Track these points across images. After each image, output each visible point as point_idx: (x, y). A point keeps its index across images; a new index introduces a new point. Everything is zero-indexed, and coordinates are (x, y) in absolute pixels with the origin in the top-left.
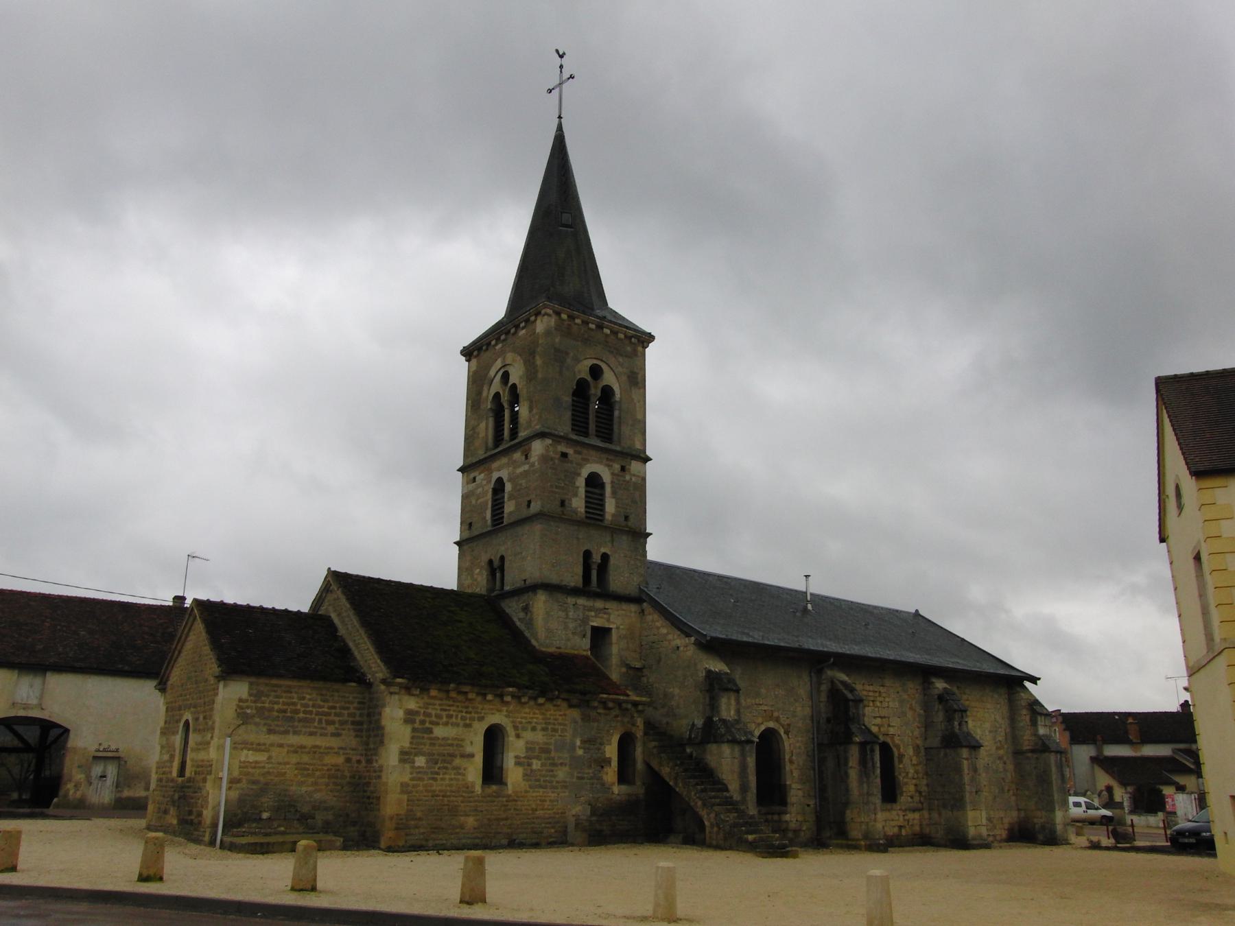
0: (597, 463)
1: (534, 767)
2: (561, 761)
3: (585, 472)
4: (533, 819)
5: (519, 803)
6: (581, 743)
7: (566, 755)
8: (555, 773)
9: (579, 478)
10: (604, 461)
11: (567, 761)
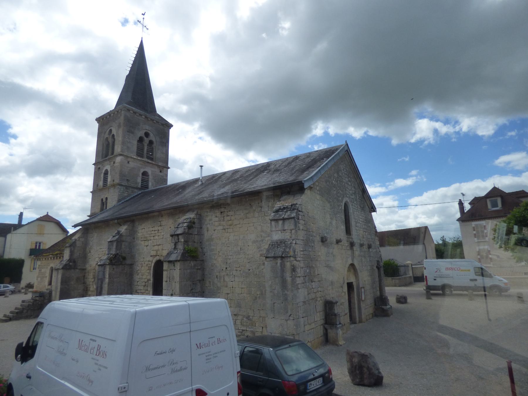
3: (142, 171)
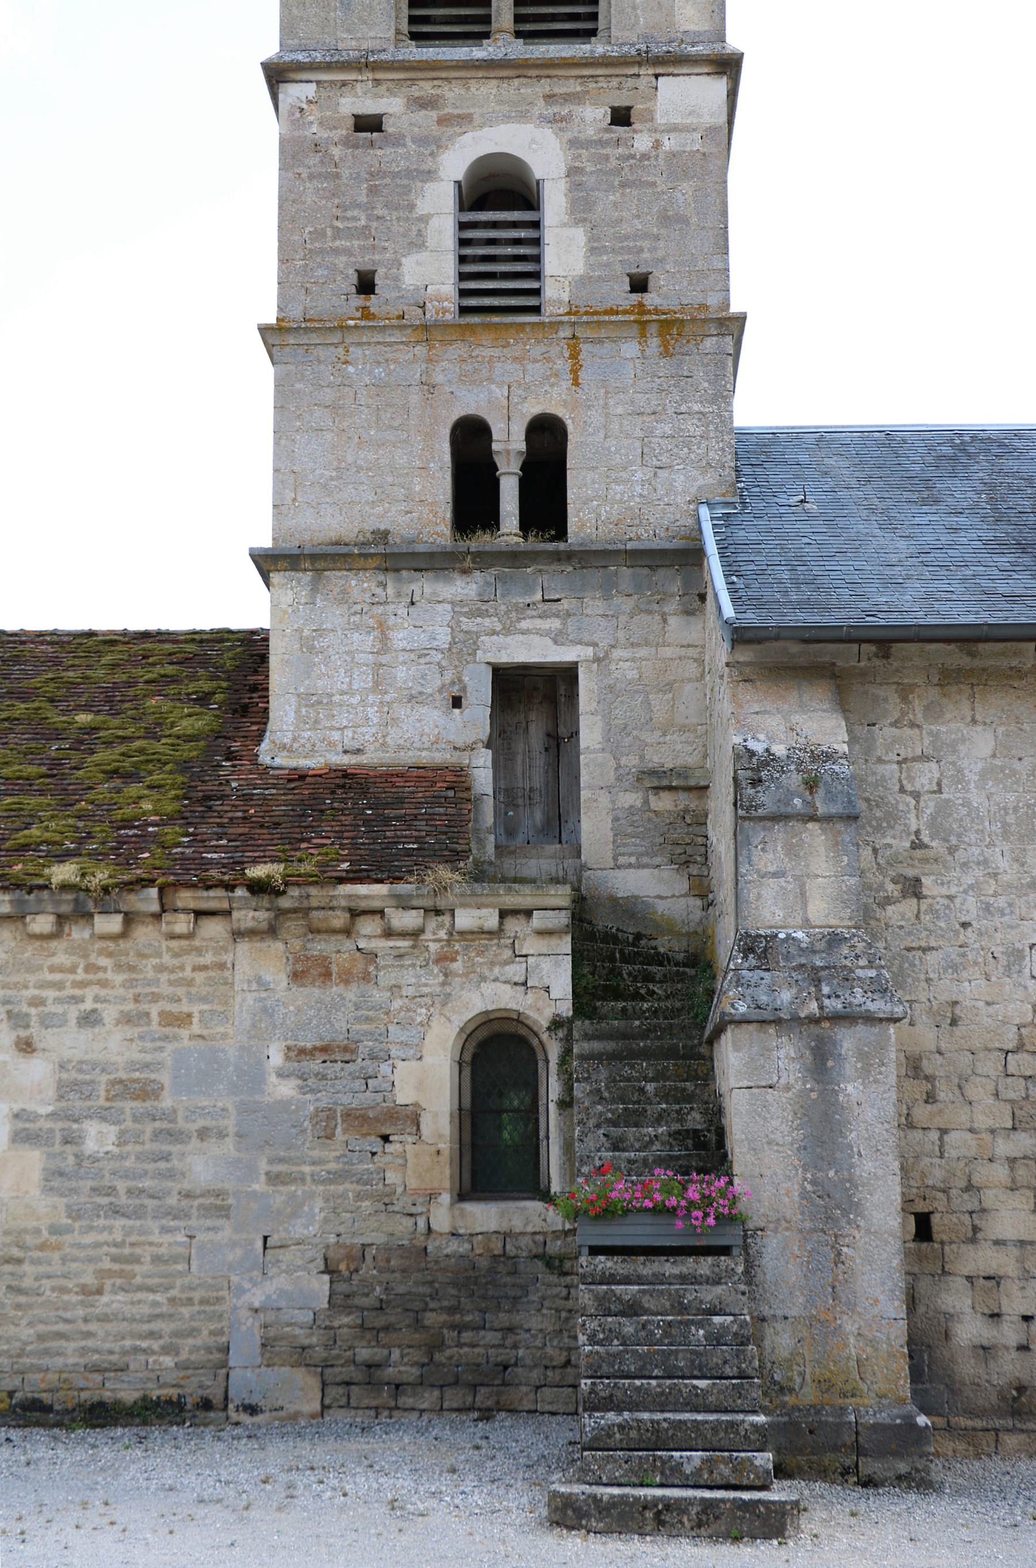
0: (507, 119)
1: (90, 1146)
2: (201, 1123)
4: (86, 1320)
5: (27, 1268)
6: (288, 1058)
7: (228, 1102)
8: (175, 1162)
9: (430, 187)
10: (540, 107)
11: (230, 1124)
